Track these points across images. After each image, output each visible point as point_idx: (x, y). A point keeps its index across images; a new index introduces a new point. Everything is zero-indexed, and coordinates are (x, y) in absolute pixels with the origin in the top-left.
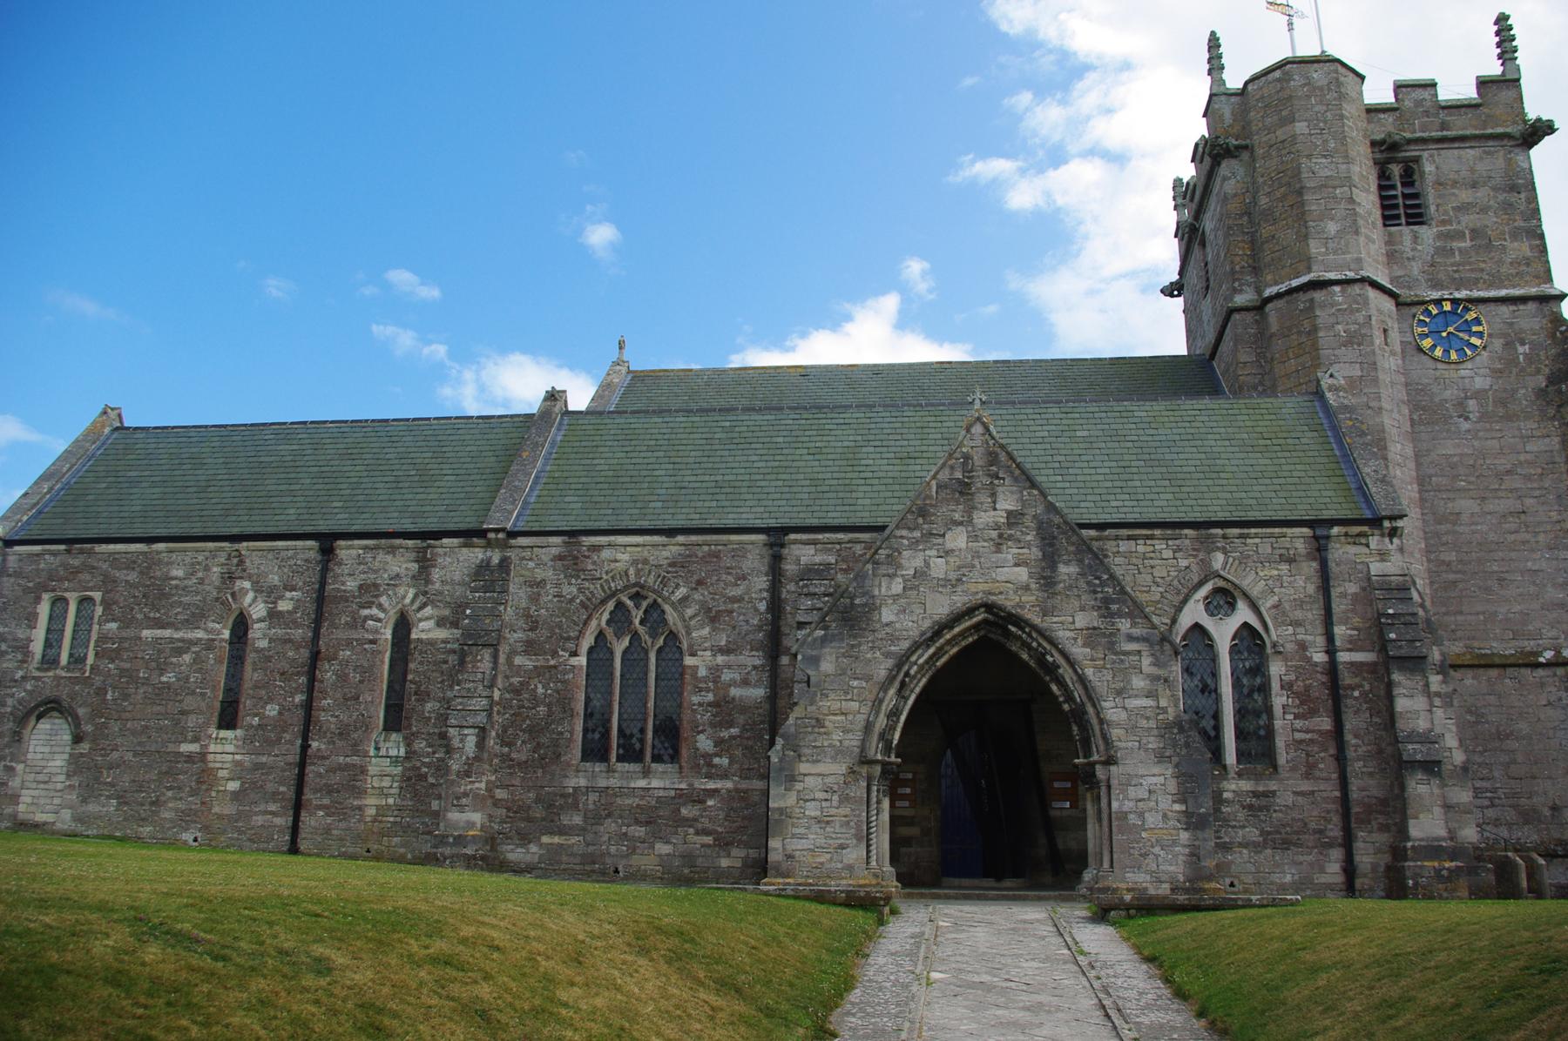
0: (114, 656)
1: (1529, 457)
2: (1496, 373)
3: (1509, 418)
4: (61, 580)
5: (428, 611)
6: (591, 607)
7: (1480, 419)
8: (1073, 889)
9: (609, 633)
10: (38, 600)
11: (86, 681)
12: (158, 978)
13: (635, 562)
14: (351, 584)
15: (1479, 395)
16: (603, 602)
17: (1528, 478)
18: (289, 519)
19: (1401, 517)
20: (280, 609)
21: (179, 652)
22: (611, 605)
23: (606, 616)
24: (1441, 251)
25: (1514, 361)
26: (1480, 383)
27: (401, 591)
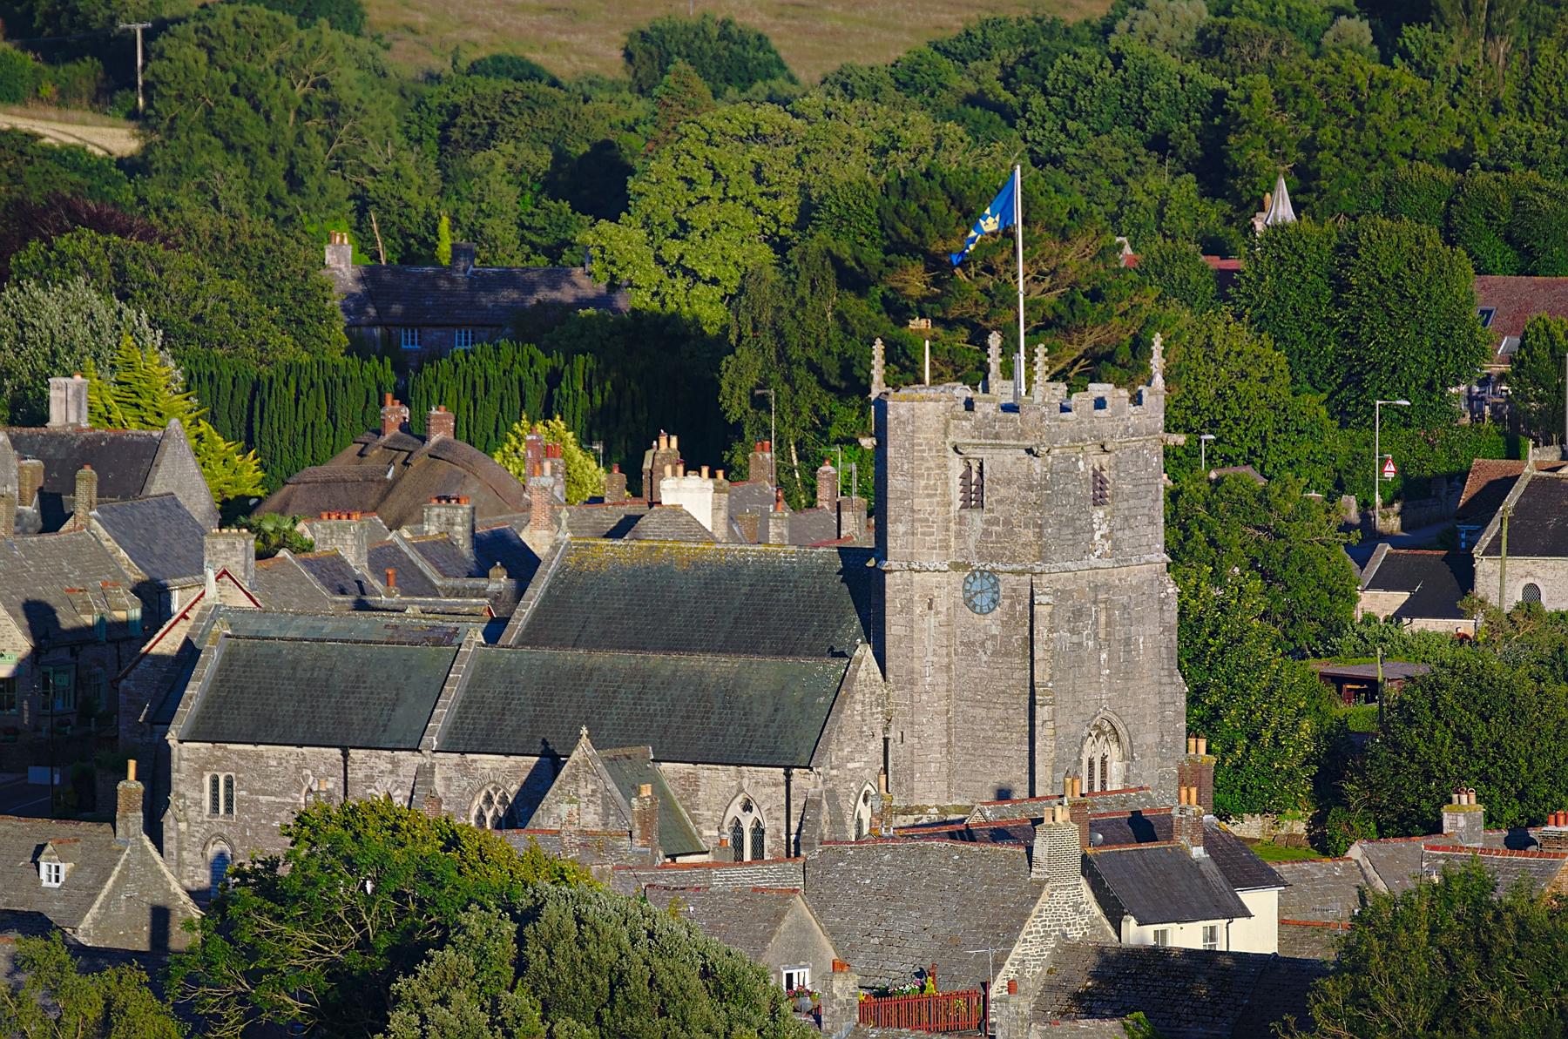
0: (247, 811)
1: (1014, 682)
2: (1004, 624)
3: (1007, 654)
4: (211, 764)
5: (399, 792)
6: (474, 794)
7: (992, 655)
8: (170, 615)
9: (484, 807)
10: (202, 776)
11: (235, 825)
12: (1201, 34)
13: (492, 769)
14: (361, 775)
15: (994, 637)
16: (480, 790)
17: (1011, 695)
18: (338, 743)
19: (154, 830)
20: (31, 780)
21: (280, 809)
22: (483, 793)
23: (482, 799)
24: (986, 533)
25: (1013, 617)
26: (995, 630)
27: (385, 780)
